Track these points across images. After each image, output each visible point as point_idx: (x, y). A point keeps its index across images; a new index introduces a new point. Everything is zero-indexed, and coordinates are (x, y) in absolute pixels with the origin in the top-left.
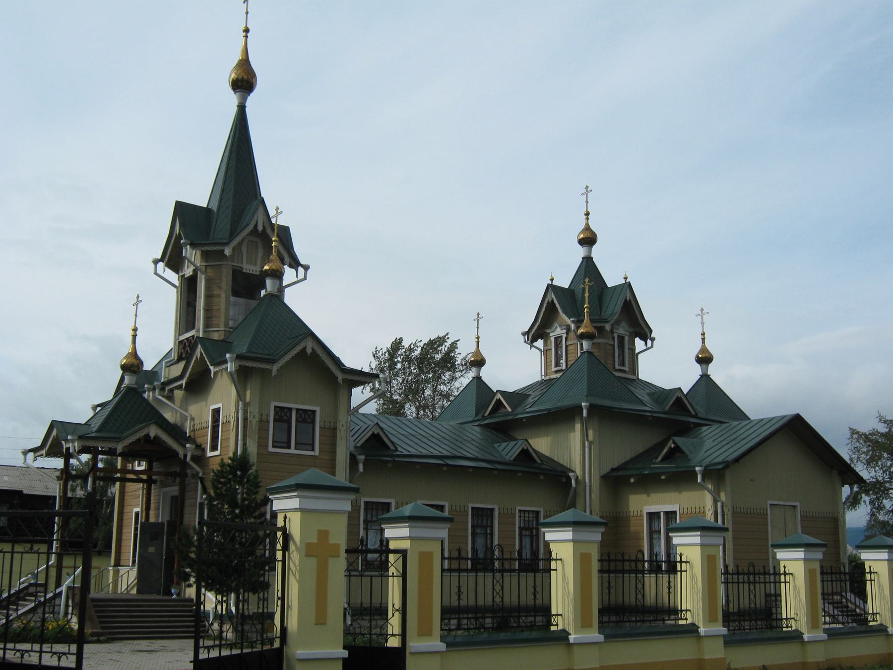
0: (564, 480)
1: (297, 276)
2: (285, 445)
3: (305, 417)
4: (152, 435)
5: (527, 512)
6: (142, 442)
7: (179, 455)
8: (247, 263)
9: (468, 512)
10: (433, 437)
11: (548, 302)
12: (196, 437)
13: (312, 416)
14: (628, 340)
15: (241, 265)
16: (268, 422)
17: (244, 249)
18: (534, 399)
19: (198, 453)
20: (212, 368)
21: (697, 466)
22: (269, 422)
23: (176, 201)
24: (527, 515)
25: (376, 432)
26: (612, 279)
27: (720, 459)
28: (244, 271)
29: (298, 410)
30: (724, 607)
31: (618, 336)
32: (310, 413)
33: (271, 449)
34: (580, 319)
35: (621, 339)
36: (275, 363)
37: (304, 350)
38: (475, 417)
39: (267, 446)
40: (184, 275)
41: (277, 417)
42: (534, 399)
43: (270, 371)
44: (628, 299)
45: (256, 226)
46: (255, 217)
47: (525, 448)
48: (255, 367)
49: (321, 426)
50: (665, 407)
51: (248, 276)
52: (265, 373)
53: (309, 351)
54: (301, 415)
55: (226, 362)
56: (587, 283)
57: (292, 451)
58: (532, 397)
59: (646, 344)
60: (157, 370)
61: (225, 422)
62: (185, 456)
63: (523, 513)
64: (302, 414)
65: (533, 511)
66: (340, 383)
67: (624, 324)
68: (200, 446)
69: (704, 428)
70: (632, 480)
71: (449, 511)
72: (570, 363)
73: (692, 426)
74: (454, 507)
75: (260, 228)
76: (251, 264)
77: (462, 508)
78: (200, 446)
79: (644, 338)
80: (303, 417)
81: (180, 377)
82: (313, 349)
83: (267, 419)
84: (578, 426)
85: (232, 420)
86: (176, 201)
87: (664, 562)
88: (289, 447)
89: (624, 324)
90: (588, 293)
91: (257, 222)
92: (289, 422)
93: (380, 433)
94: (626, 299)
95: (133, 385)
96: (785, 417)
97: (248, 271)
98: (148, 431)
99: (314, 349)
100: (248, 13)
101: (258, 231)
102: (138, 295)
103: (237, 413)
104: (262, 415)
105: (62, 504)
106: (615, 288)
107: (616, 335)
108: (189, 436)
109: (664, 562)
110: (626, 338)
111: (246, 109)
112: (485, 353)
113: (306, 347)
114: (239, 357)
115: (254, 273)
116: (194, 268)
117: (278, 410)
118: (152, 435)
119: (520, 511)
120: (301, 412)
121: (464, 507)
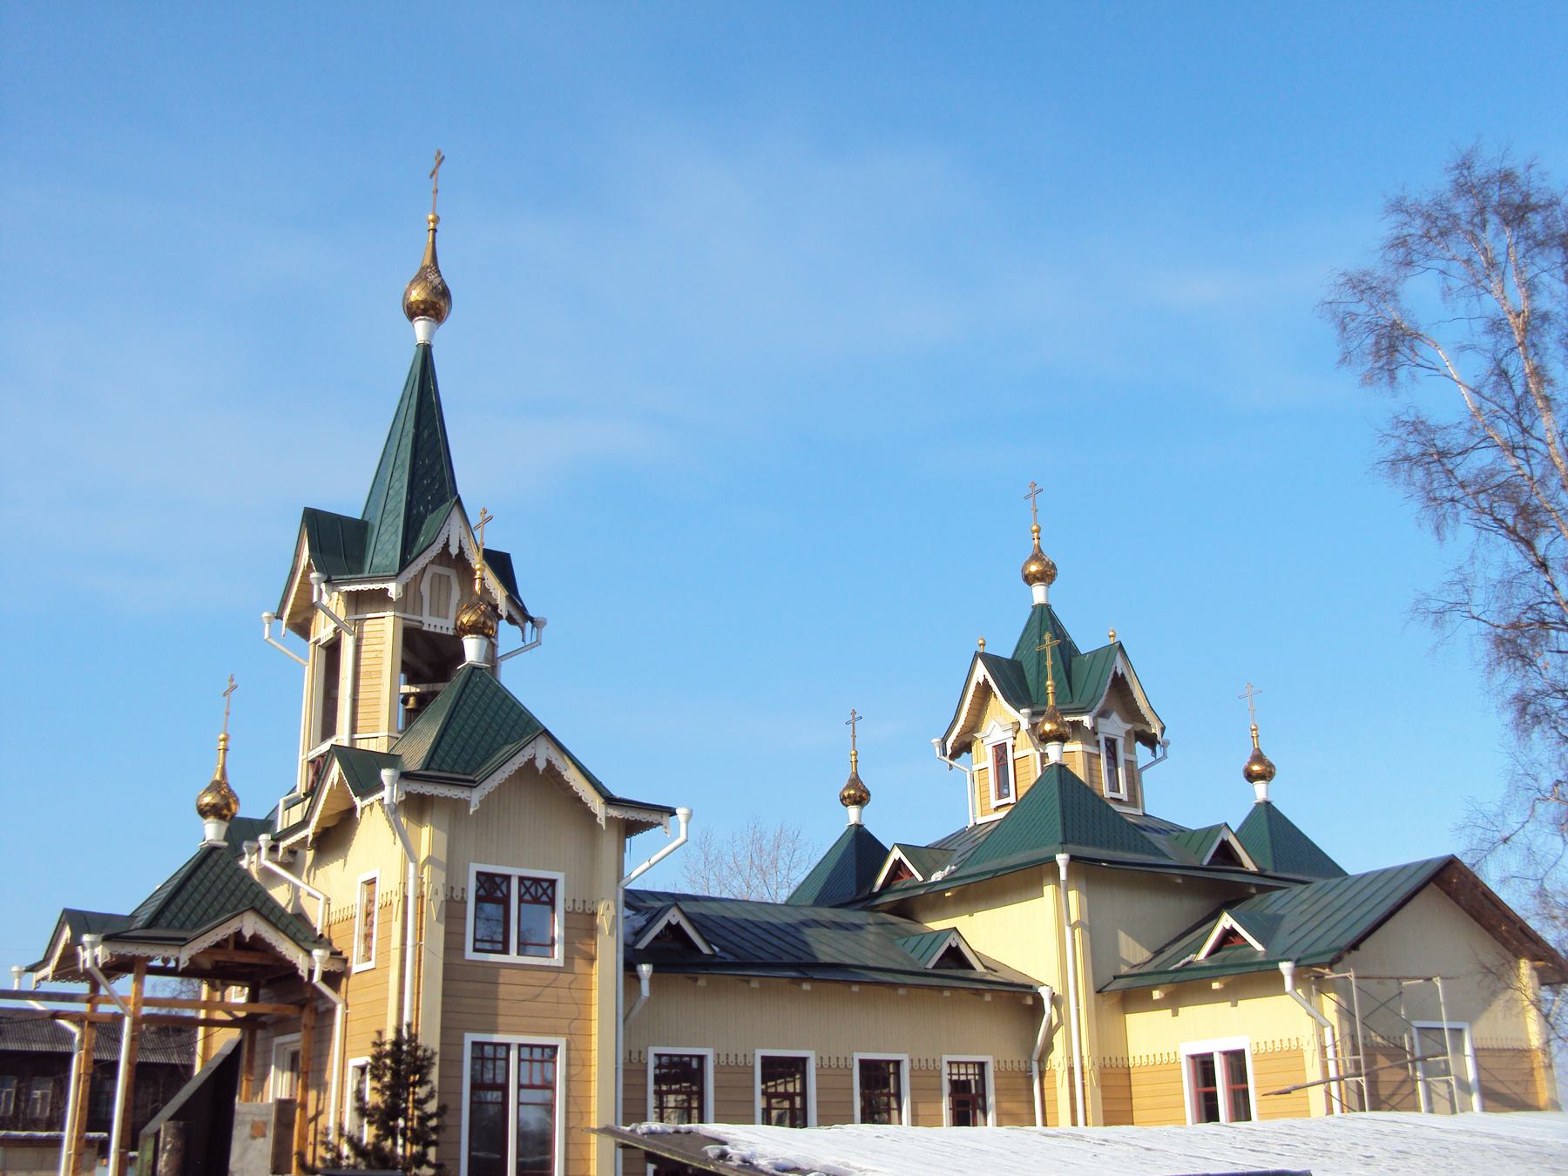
0: (1029, 1001)
1: (523, 641)
2: (500, 947)
3: (536, 889)
4: (248, 933)
5: (956, 1065)
6: (231, 946)
7: (300, 972)
8: (430, 615)
9: (852, 1069)
10: (795, 947)
11: (978, 683)
12: (333, 937)
13: (549, 892)
14: (1124, 746)
15: (419, 618)
16: (464, 902)
17: (425, 588)
18: (963, 857)
19: (335, 967)
20: (357, 800)
21: (1282, 961)
22: (466, 903)
23: (307, 510)
24: (955, 1071)
25: (674, 922)
26: (1086, 641)
27: (1321, 946)
28: (425, 628)
29: (522, 879)
30: (894, 1105)
31: (1107, 740)
32: (545, 885)
33: (470, 954)
34: (1037, 708)
35: (1111, 745)
36: (475, 787)
37: (532, 761)
38: (857, 894)
39: (463, 950)
40: (319, 640)
41: (482, 892)
42: (963, 857)
43: (467, 803)
44: (1119, 673)
45: (447, 545)
46: (445, 531)
47: (954, 945)
48: (437, 796)
49: (568, 910)
50: (1202, 860)
51: (433, 640)
52: (459, 806)
53: (541, 765)
54: (528, 890)
55: (381, 787)
56: (1048, 642)
57: (513, 957)
58: (959, 854)
59: (1154, 751)
60: (272, 819)
61: (384, 904)
62: (311, 973)
63: (954, 1066)
64: (541, 896)
65: (974, 1063)
66: (601, 825)
67: (1115, 717)
68: (340, 953)
69: (1277, 894)
70: (1157, 995)
71: (817, 1069)
72: (1019, 798)
73: (1253, 890)
74: (826, 1061)
75: (454, 550)
76: (438, 616)
77: (842, 1062)
78: (340, 953)
79: (1150, 741)
80: (533, 893)
81: (304, 824)
82: (549, 762)
83: (463, 898)
84: (1049, 890)
85: (395, 900)
86: (307, 510)
87: (894, 1109)
88: (505, 951)
89: (1115, 717)
90: (1052, 660)
91: (448, 539)
92: (505, 902)
93: (681, 923)
94: (1116, 673)
95: (219, 840)
96: (1428, 862)
97: (432, 629)
98: (240, 925)
99: (551, 762)
100: (437, 191)
101: (450, 555)
102: (232, 675)
103: (404, 887)
104: (452, 888)
105: (82, 1071)
106: (1095, 654)
107: (1101, 738)
108: (321, 936)
109: (894, 1109)
110: (1120, 744)
111: (433, 350)
112: (867, 782)
113: (534, 758)
114: (406, 776)
115: (444, 631)
116: (336, 625)
117: (483, 879)
118: (248, 933)
119: (950, 1063)
120: (528, 883)
121: (846, 1058)
